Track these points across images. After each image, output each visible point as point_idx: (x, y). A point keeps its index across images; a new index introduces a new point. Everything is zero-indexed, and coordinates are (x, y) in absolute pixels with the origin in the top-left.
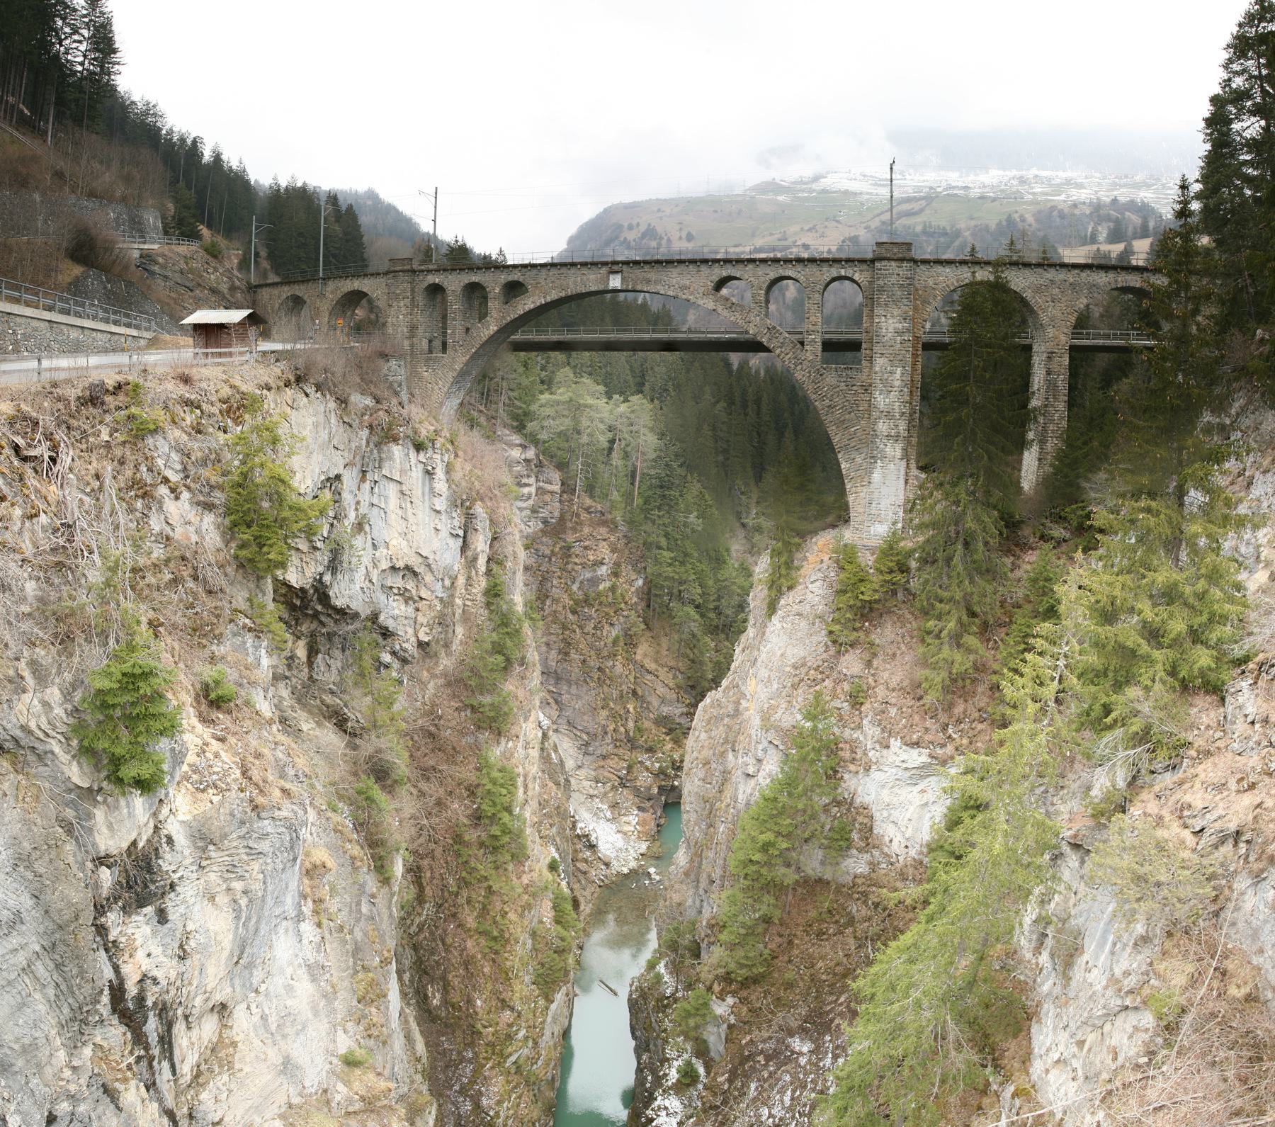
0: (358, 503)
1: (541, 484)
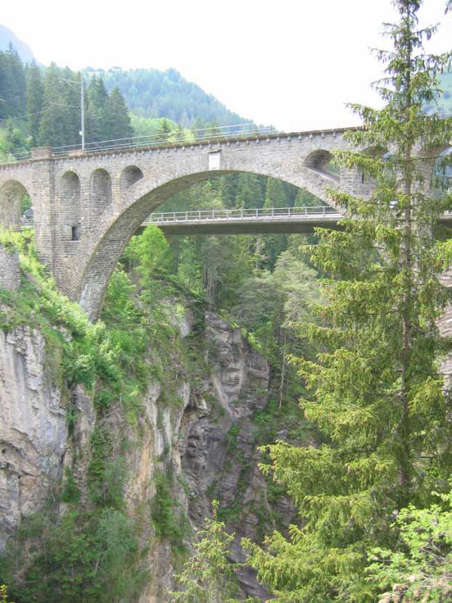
1: (251, 369)
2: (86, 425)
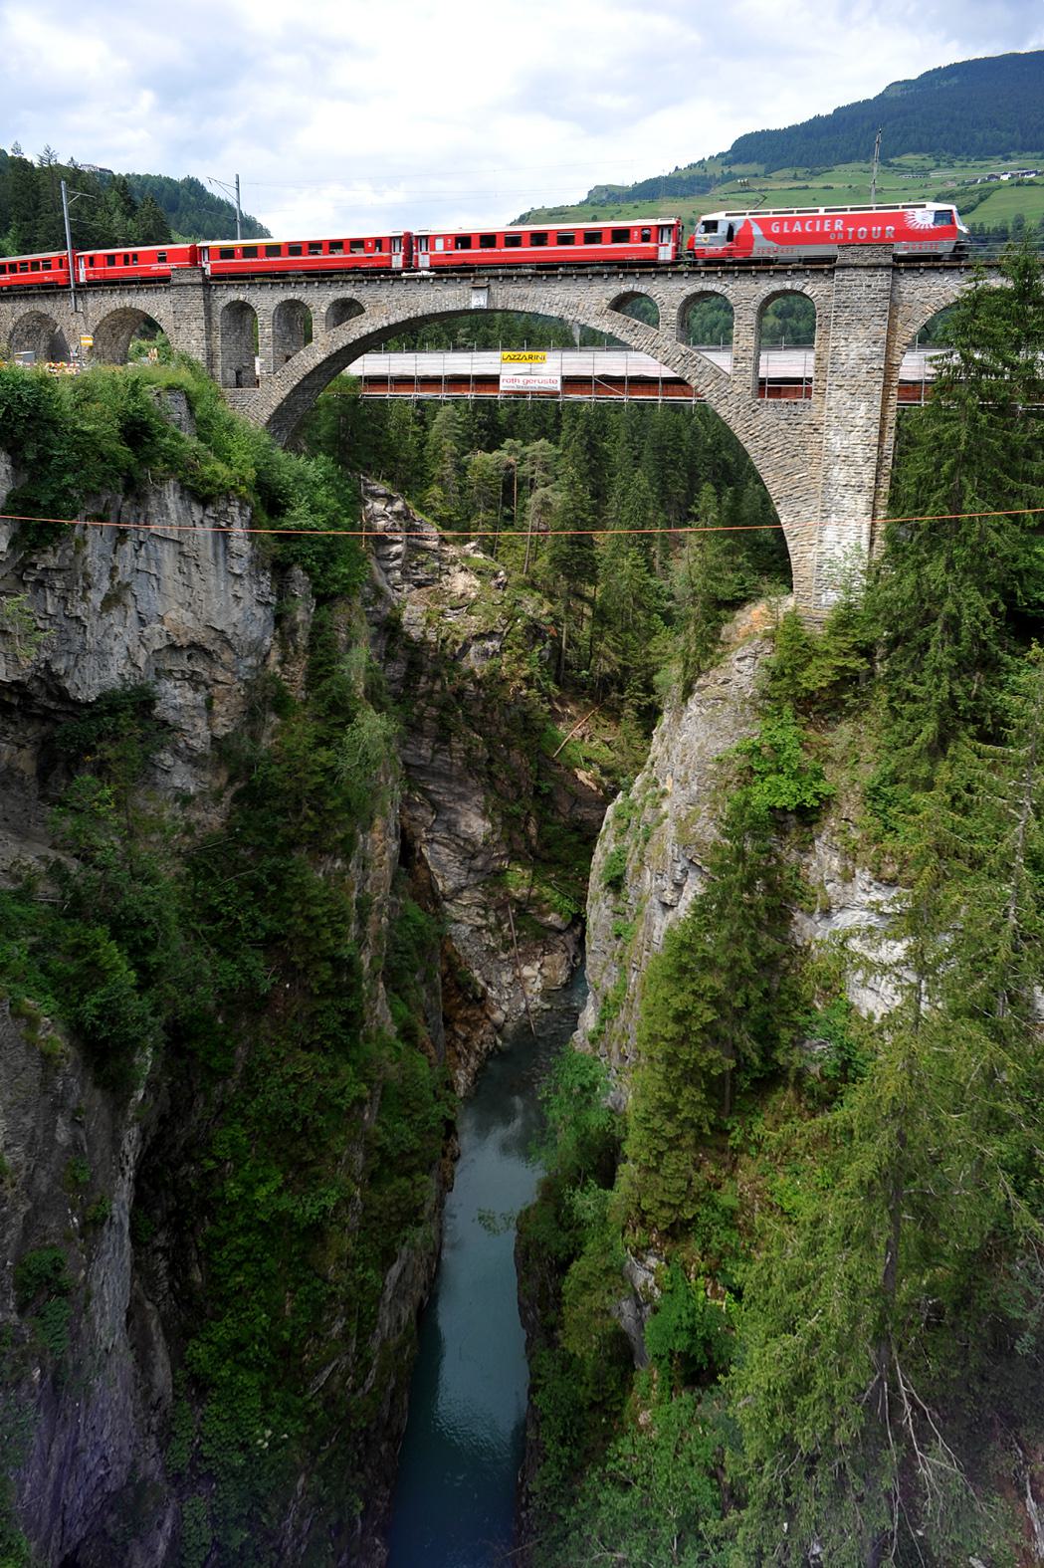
0: (114, 569)
2: (302, 614)
